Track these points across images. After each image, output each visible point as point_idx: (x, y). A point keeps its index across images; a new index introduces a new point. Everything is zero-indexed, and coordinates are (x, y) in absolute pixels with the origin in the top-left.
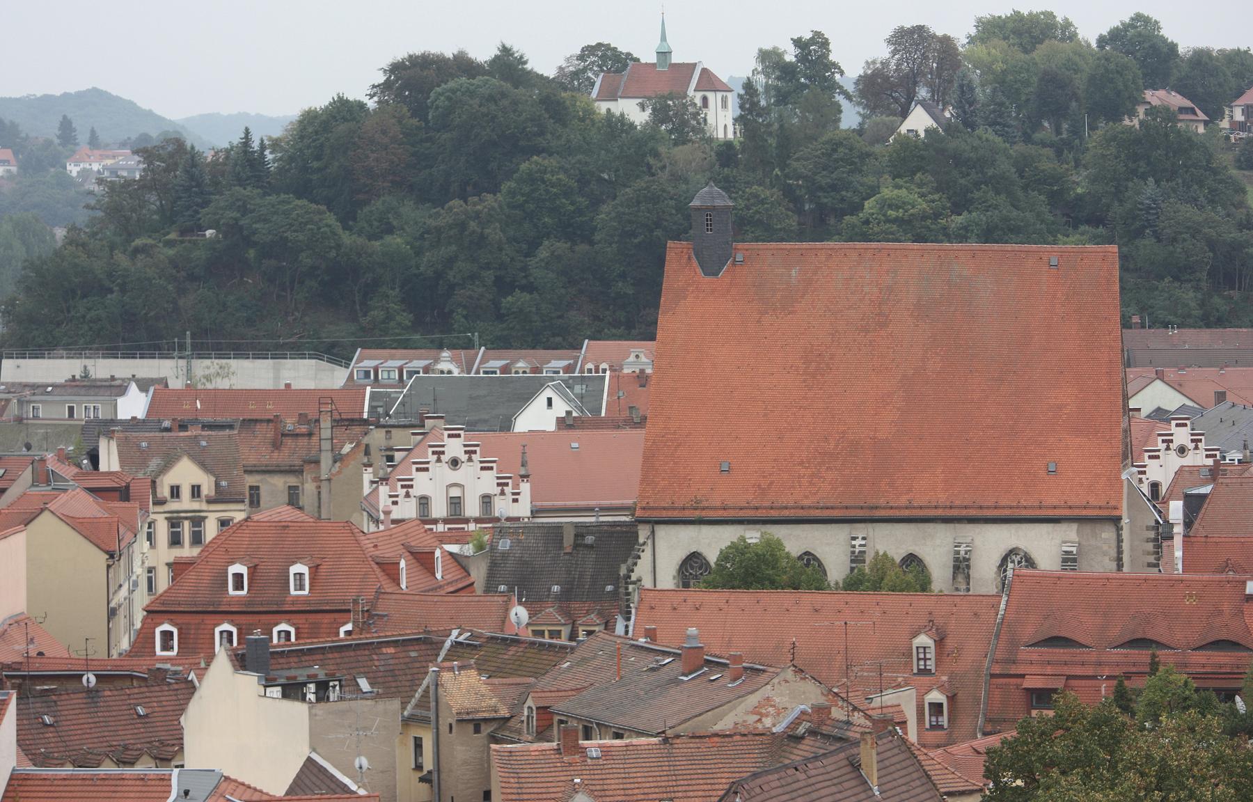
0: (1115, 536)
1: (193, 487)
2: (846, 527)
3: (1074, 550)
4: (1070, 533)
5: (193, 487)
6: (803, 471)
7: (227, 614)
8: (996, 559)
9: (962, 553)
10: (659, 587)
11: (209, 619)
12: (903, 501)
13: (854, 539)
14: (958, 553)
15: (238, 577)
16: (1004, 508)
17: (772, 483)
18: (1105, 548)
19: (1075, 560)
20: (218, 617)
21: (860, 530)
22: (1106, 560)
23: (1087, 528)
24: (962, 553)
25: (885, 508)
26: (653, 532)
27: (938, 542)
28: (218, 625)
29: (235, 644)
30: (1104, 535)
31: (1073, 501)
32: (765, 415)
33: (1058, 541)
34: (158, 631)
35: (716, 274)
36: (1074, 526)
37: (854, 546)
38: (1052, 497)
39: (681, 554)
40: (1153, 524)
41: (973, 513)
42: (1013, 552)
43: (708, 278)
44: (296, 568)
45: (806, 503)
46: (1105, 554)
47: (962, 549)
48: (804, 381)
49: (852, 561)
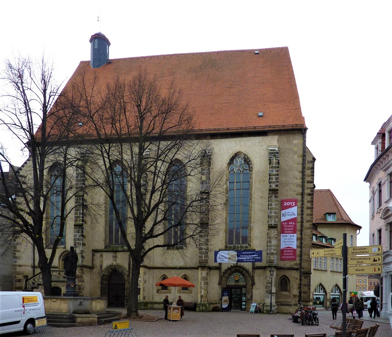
4: (273, 142)
8: (226, 159)
18: (295, 149)
22: (296, 157)
23: (284, 138)
30: (295, 142)
40: (311, 160)
42: (236, 155)
46: (295, 153)
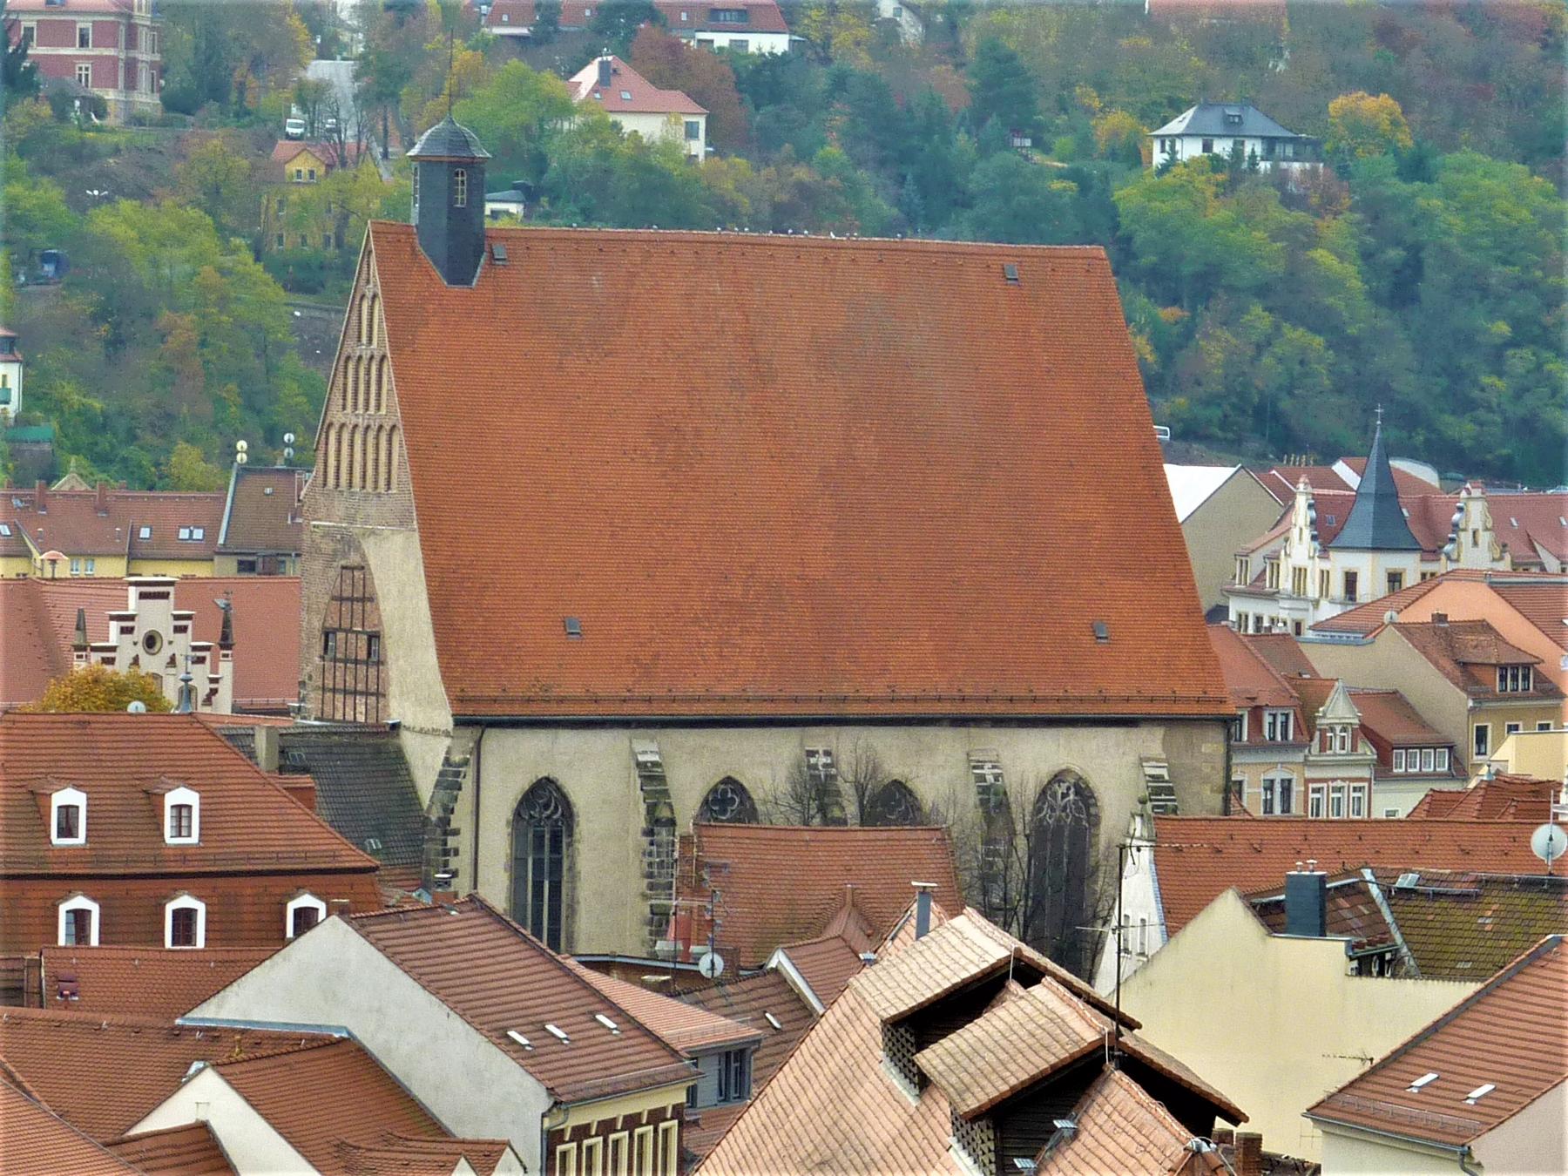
0: (1222, 750)
1: (1347, 574)
2: (794, 733)
3: (1164, 772)
4: (1151, 741)
5: (1347, 574)
6: (703, 635)
7: (71, 880)
9: (990, 779)
10: (1373, 817)
11: (277, 885)
12: (879, 688)
13: (812, 754)
14: (982, 778)
15: (68, 812)
16: (1045, 700)
17: (656, 656)
18: (1207, 770)
19: (1170, 791)
20: (170, 883)
21: (820, 739)
22: (1207, 791)
23: (1180, 735)
24: (990, 779)
25: (855, 700)
26: (478, 743)
27: (940, 759)
28: (65, 898)
29: (94, 940)
30: (1207, 748)
31: (1150, 689)
32: (613, 535)
33: (1132, 758)
34: (63, 908)
35: (466, 281)
36: (1159, 732)
37: (815, 767)
38: (1118, 684)
39: (521, 783)
41: (1000, 709)
43: (457, 289)
44: (68, 796)
45: (721, 690)
46: (1205, 780)
47: (987, 771)
48: (664, 475)
49: (666, 793)
